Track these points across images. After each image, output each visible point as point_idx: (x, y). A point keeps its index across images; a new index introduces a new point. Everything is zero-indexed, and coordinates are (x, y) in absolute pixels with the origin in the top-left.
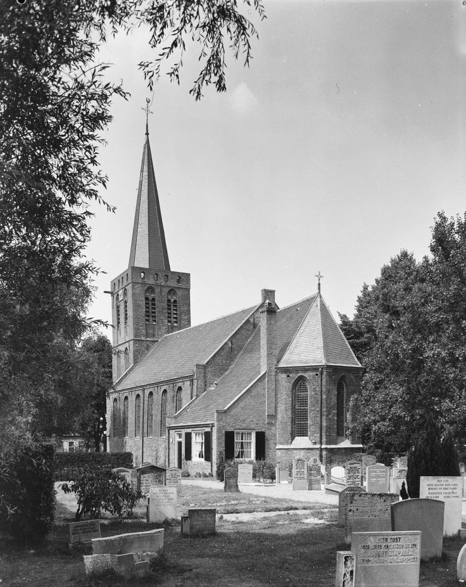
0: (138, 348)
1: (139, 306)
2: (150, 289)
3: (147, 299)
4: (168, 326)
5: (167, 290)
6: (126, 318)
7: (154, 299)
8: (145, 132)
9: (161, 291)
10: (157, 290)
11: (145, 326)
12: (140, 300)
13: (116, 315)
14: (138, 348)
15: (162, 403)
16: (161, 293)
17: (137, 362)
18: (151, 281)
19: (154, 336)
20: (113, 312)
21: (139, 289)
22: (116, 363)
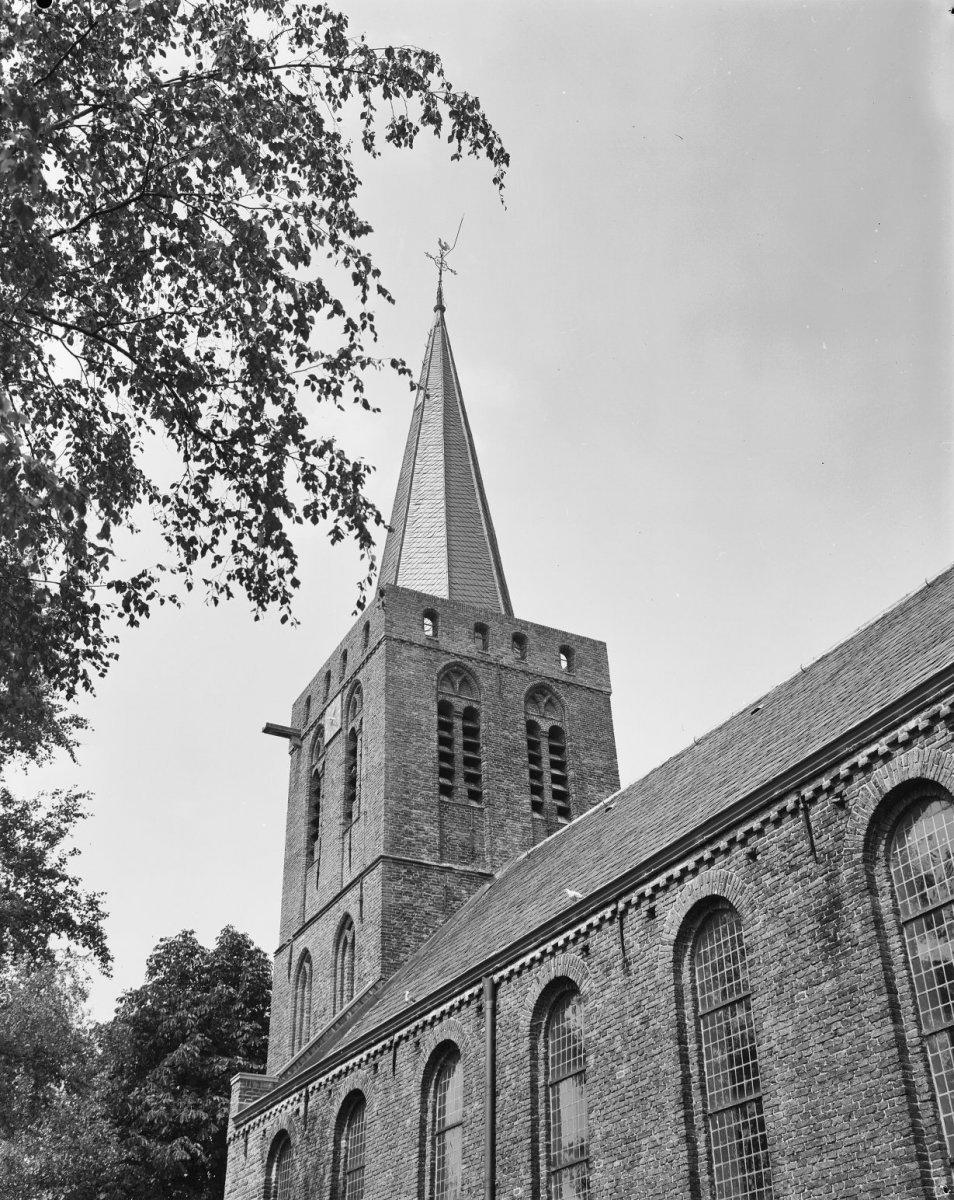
0: (406, 899)
1: (412, 726)
2: (457, 673)
3: (444, 708)
4: (534, 820)
5: (520, 687)
6: (351, 797)
7: (470, 714)
8: (435, 303)
9: (501, 686)
10: (486, 680)
11: (436, 811)
12: (416, 707)
13: (303, 798)
14: (406, 899)
15: (681, 1026)
16: (500, 693)
17: (397, 966)
18: (463, 645)
19: (473, 856)
20: (292, 803)
21: (415, 668)
22: (287, 1013)
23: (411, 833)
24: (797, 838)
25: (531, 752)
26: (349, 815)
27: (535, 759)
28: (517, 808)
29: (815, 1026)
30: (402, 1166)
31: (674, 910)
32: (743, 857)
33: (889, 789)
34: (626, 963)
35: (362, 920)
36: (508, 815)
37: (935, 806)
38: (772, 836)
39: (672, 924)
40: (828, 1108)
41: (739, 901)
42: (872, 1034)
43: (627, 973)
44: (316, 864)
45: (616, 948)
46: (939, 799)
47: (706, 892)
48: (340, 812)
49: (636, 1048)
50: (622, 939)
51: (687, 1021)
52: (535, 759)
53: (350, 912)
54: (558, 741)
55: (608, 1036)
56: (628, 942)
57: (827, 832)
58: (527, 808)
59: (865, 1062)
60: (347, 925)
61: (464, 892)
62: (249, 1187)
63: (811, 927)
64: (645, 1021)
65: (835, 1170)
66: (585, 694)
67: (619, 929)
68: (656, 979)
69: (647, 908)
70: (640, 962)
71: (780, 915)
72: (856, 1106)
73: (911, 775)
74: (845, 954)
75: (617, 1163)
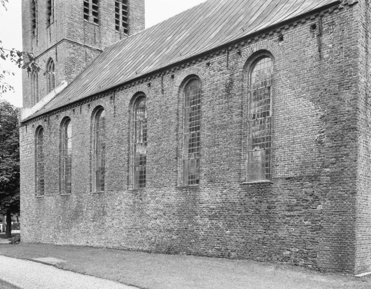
0: (73, 55)
14: (73, 55)
23: (74, 32)
24: (223, 61)
25: (116, 7)
26: (49, 21)
27: (117, 10)
28: (110, 27)
29: (219, 115)
30: (84, 139)
31: (181, 76)
32: (205, 64)
33: (255, 51)
34: (163, 90)
35: (57, 60)
36: (107, 29)
37: (266, 59)
38: (215, 59)
39: (179, 81)
40: (219, 136)
41: (202, 77)
42: (235, 119)
43: (163, 93)
44: (36, 37)
45: (160, 86)
46: (268, 57)
47: (192, 72)
48: (45, 19)
49: (164, 115)
50: (162, 83)
51: (180, 109)
52: (117, 10)
53: (52, 57)
54: (125, 4)
55: (155, 111)
56: (164, 84)
57: (233, 61)
58: (114, 28)
59: (231, 126)
60: (50, 62)
61: (92, 55)
62: (29, 140)
63: (223, 88)
64: (167, 108)
65: (217, 151)
66: (202, 32)
67: (161, 79)
68: (172, 96)
69: (171, 75)
70: (167, 91)
71: (214, 83)
72: (226, 136)
73: (263, 48)
74: (231, 97)
75: (155, 144)
